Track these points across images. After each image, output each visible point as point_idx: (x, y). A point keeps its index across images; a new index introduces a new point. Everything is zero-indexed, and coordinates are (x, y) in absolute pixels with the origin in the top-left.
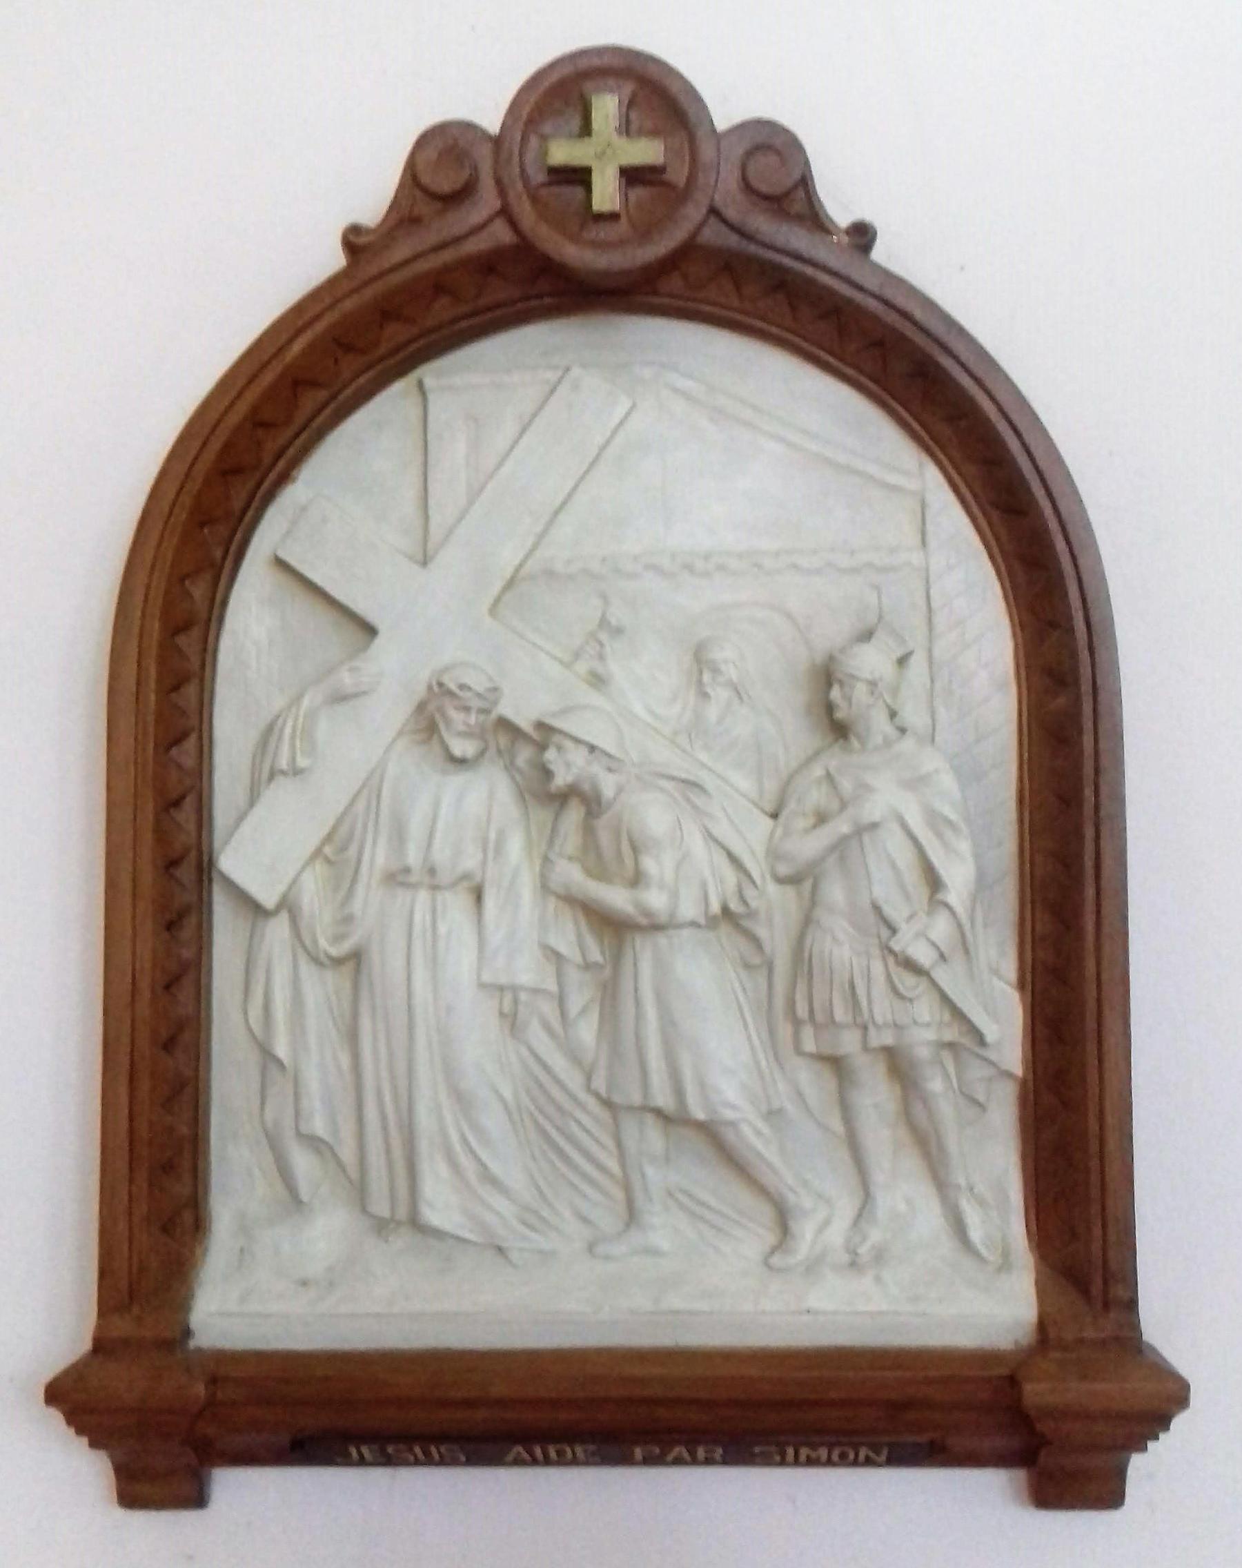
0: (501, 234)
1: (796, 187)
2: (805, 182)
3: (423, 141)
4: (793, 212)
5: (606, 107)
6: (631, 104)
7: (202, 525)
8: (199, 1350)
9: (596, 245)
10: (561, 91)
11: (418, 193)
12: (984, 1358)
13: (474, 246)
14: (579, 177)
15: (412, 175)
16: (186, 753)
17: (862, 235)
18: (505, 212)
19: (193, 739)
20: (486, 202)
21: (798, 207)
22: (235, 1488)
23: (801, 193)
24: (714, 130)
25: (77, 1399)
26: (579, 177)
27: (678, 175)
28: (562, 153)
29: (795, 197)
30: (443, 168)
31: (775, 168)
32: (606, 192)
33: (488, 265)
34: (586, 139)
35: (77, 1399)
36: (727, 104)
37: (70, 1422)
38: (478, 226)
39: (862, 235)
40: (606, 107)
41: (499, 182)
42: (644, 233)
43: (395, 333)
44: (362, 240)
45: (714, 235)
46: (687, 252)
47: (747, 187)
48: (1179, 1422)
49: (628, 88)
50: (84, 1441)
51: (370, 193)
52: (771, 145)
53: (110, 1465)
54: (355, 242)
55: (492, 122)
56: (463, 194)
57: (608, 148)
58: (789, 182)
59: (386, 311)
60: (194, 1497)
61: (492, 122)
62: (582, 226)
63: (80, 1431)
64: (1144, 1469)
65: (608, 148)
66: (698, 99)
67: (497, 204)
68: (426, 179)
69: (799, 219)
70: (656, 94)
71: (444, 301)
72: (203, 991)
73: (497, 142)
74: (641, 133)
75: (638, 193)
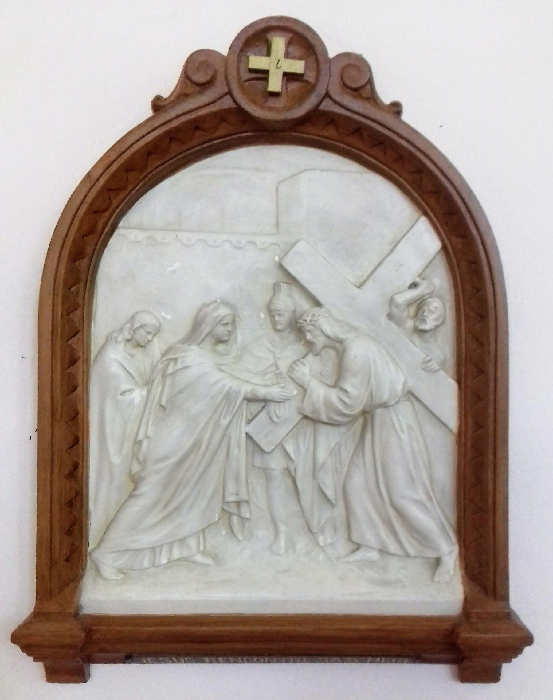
0: (227, 103)
1: (366, 84)
2: (370, 82)
4: (364, 95)
5: (279, 43)
8: (85, 615)
9: (270, 109)
10: (256, 37)
11: (189, 83)
15: (186, 76)
16: (76, 316)
17: (396, 108)
19: (80, 309)
20: (219, 88)
21: (366, 92)
22: (99, 672)
23: (368, 87)
25: (26, 639)
27: (311, 77)
28: (257, 62)
29: (365, 90)
30: (200, 71)
31: (355, 75)
32: (275, 84)
33: (222, 116)
35: (26, 639)
39: (396, 108)
40: (279, 43)
41: (226, 78)
42: (300, 99)
43: (175, 147)
44: (161, 103)
46: (315, 117)
48: (527, 650)
49: (290, 35)
50: (32, 658)
51: (167, 84)
53: (43, 666)
54: (158, 105)
55: (224, 50)
57: (278, 62)
58: (363, 83)
59: (172, 136)
60: (79, 675)
61: (224, 50)
62: (266, 100)
63: (29, 654)
64: (506, 669)
65: (278, 62)
66: (309, 28)
68: (190, 74)
69: (367, 99)
70: (302, 40)
71: (198, 133)
72: (85, 451)
73: (225, 60)
74: (293, 58)
75: (294, 86)
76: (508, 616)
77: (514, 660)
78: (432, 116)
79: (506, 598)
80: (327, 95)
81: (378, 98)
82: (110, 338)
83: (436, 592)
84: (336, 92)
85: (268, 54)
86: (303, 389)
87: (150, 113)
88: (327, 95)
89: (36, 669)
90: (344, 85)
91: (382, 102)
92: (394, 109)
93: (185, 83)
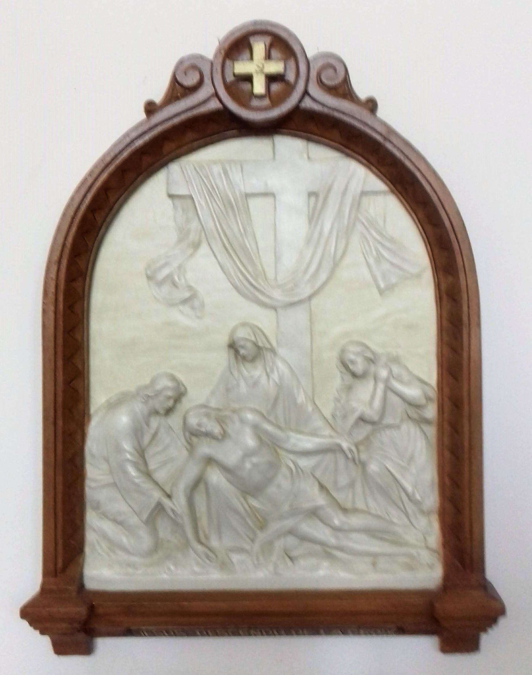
0: (214, 105)
2: (346, 80)
3: (181, 62)
5: (259, 48)
6: (271, 45)
7: (75, 256)
10: (238, 46)
12: (422, 593)
13: (203, 109)
14: (248, 79)
15: (175, 81)
17: (371, 105)
18: (216, 95)
22: (103, 644)
24: (81, 586)
25: (34, 614)
26: (248, 79)
27: (291, 77)
28: (242, 67)
29: (343, 90)
34: (61, 648)
35: (34, 614)
36: (313, 43)
37: (31, 624)
38: (204, 100)
39: (371, 105)
40: (259, 48)
42: (275, 100)
45: (308, 104)
46: (297, 110)
47: (187, 412)
48: (502, 622)
50: (37, 633)
52: (333, 63)
54: (151, 109)
56: (194, 89)
57: (258, 66)
60: (86, 649)
63: (35, 628)
67: (211, 91)
68: (179, 79)
70: (281, 44)
75: (275, 87)
76: (485, 587)
77: (490, 631)
78: (405, 115)
79: (482, 570)
80: (306, 93)
81: (355, 93)
82: (211, 555)
83: (415, 565)
84: (314, 90)
85: (252, 58)
86: (282, 518)
87: (143, 116)
88: (306, 93)
89: (46, 642)
90: (320, 83)
91: (357, 97)
92: (370, 104)
93: (174, 85)
